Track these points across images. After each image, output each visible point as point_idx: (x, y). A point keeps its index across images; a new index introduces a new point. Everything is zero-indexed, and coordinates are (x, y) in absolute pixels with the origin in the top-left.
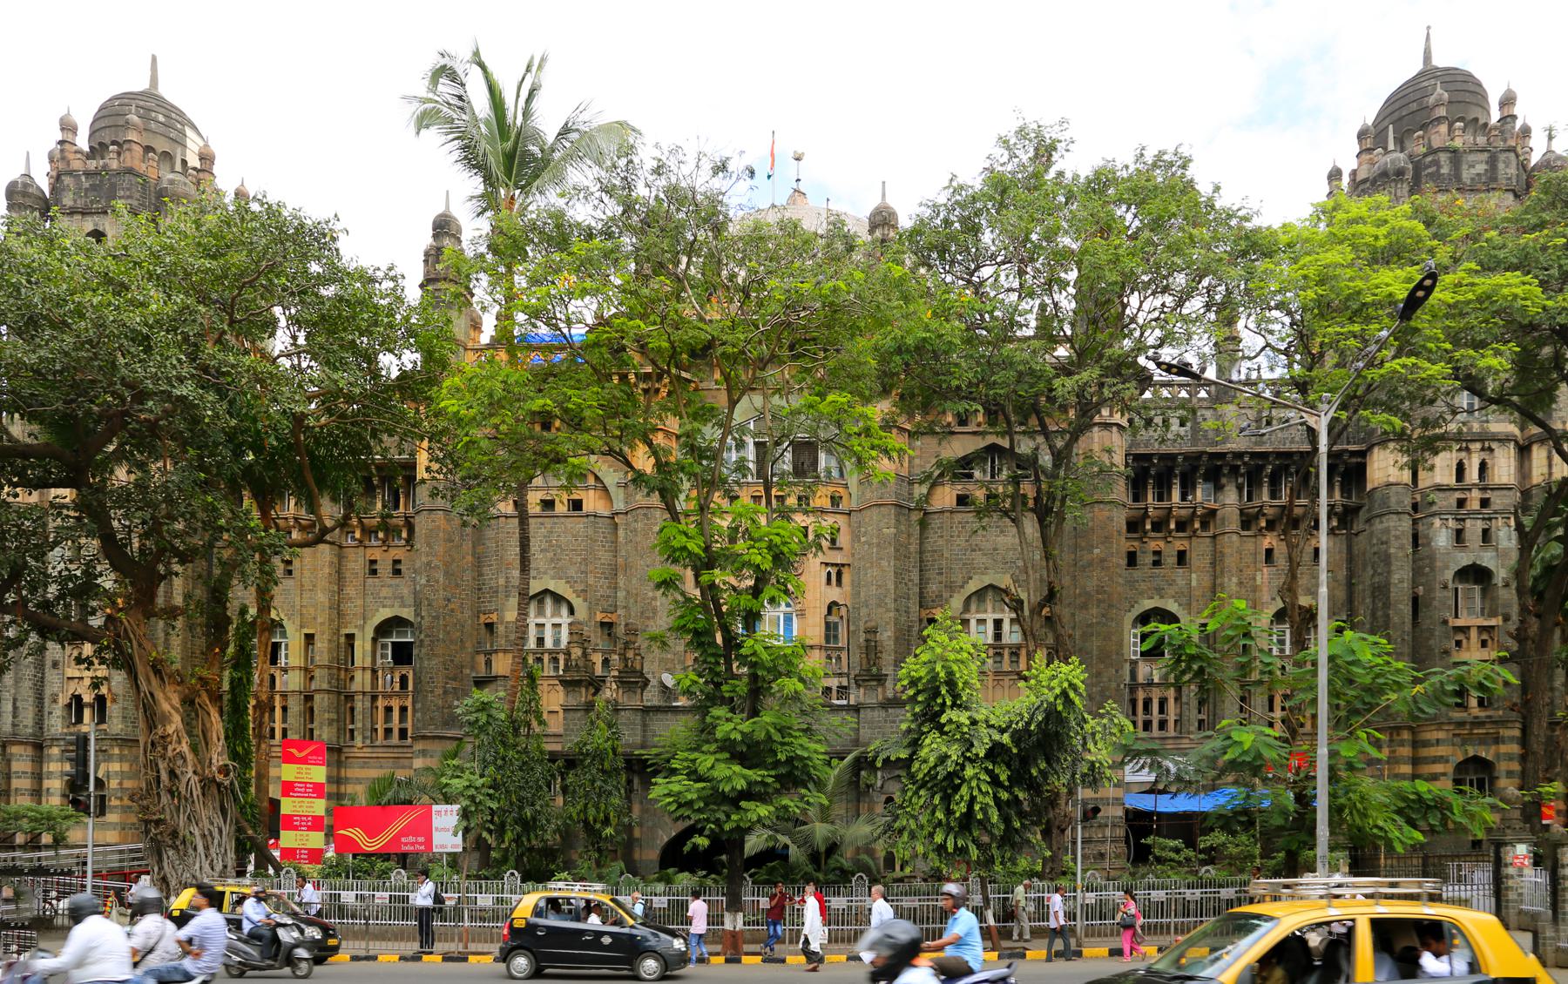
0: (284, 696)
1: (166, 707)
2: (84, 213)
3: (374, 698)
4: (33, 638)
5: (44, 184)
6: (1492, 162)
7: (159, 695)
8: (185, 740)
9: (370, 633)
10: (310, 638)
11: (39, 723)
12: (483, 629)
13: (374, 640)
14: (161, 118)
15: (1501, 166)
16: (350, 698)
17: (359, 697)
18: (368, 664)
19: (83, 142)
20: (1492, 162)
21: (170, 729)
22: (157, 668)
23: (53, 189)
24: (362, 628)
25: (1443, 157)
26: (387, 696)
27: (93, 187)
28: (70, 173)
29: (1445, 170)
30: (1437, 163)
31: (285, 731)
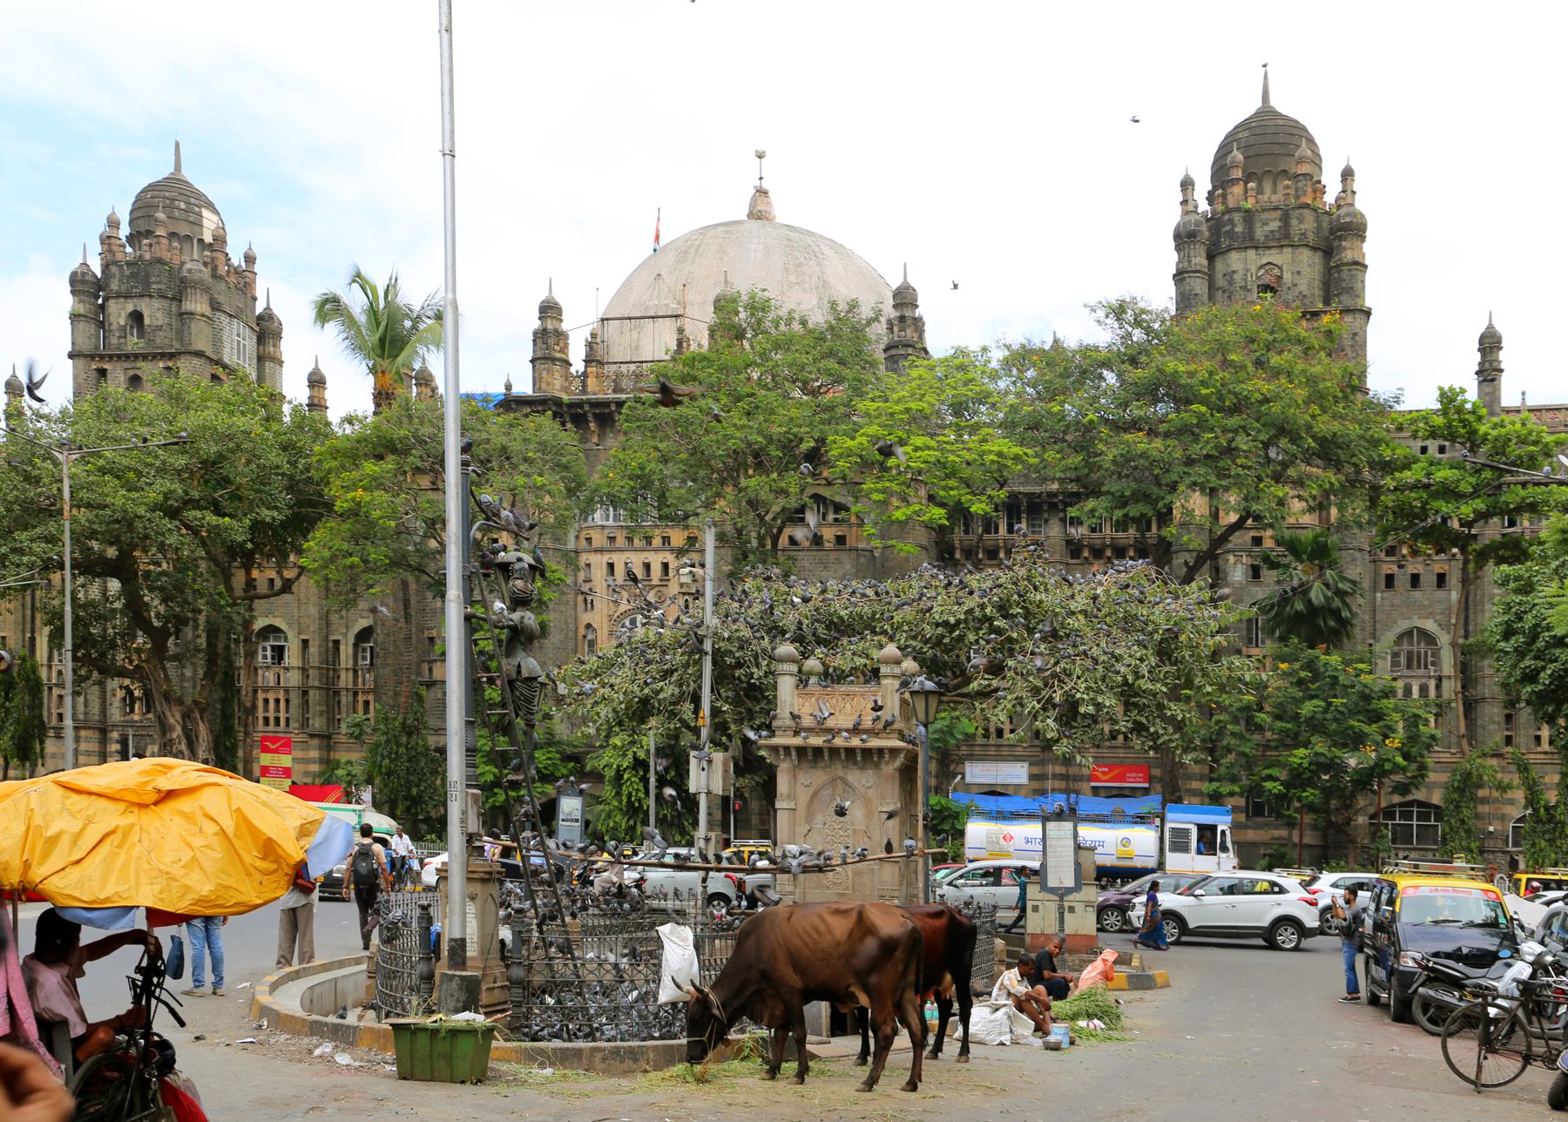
0: (287, 691)
1: (172, 721)
2: (127, 297)
3: (356, 694)
4: (95, 674)
5: (96, 268)
6: (1285, 219)
7: (168, 714)
8: (184, 742)
9: (351, 640)
10: (305, 643)
11: (103, 712)
12: (427, 643)
13: (356, 645)
14: (183, 206)
15: (1294, 222)
16: (337, 693)
17: (344, 693)
18: (350, 665)
19: (124, 231)
20: (1285, 219)
21: (174, 736)
22: (167, 696)
23: (103, 272)
24: (345, 635)
25: (1237, 217)
26: (365, 692)
27: (133, 275)
28: (116, 263)
29: (1239, 229)
30: (1231, 221)
31: (287, 719)
